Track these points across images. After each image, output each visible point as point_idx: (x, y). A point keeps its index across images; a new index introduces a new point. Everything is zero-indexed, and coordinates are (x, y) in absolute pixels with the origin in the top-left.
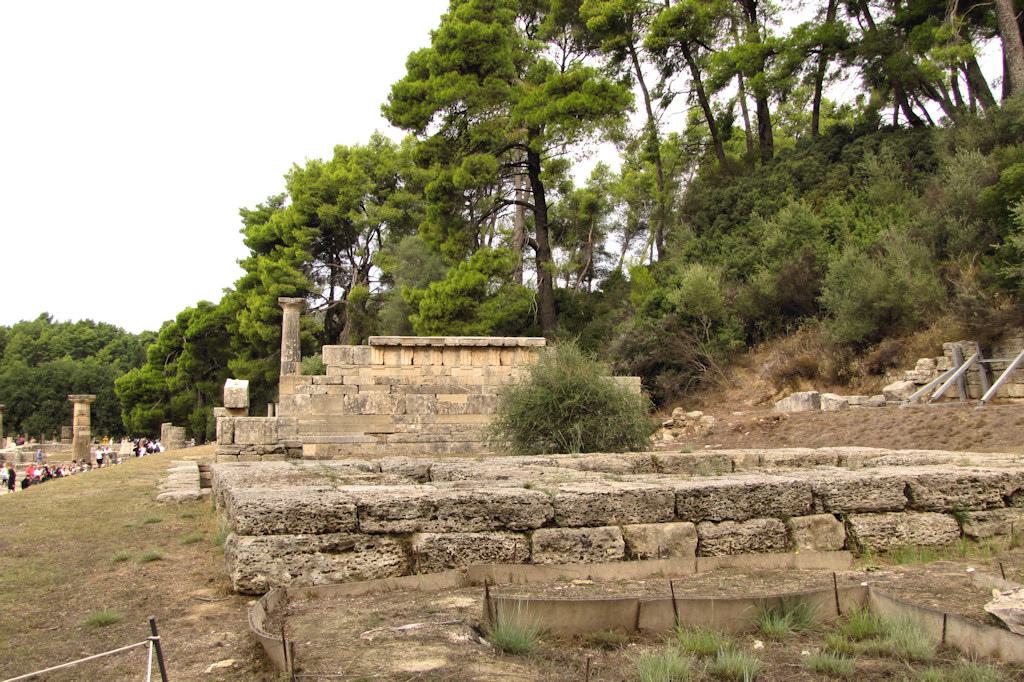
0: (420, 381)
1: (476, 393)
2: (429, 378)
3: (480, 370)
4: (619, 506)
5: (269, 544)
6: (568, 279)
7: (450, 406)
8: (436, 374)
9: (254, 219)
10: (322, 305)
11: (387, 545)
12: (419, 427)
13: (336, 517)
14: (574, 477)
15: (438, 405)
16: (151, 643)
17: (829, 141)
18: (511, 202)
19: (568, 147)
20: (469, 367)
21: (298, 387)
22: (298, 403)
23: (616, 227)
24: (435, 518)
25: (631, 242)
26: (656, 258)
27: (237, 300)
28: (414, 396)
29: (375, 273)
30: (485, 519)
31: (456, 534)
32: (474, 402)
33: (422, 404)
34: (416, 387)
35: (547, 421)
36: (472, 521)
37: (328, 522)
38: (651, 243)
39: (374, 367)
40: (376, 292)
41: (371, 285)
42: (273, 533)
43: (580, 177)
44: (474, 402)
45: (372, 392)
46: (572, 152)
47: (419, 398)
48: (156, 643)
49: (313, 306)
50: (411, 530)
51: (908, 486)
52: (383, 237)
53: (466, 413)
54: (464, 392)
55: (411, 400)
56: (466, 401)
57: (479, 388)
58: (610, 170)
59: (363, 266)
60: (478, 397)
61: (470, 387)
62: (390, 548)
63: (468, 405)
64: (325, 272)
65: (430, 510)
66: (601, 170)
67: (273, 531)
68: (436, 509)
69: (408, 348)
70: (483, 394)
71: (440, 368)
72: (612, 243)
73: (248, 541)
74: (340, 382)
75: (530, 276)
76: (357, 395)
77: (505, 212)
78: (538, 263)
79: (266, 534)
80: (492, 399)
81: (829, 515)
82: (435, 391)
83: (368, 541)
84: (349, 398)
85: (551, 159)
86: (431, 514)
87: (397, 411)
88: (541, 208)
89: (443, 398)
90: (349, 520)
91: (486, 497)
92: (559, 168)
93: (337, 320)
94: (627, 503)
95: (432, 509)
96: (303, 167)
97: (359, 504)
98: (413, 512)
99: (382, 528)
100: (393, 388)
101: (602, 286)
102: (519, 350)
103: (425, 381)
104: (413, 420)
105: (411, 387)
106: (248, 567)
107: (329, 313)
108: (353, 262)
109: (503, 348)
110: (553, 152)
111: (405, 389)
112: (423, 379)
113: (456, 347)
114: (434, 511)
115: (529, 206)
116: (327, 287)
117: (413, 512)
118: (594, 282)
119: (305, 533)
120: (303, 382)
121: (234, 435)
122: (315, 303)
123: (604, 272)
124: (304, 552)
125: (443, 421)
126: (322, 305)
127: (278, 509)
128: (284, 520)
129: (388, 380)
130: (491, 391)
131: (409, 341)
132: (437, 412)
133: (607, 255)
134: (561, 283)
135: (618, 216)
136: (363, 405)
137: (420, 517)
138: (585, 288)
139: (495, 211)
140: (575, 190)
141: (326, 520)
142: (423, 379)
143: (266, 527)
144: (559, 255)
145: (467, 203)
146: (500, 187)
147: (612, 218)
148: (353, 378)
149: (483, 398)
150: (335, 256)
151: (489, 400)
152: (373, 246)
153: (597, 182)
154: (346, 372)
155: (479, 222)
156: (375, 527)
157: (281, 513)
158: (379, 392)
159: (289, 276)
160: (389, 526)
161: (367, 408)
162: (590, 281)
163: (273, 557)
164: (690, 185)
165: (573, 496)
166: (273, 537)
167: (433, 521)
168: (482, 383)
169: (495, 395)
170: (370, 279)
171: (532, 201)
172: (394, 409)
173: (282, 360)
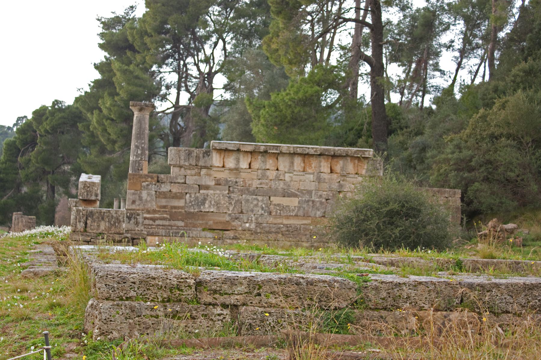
1: (307, 197)
2: (264, 181)
3: (312, 176)
4: (413, 295)
5: (123, 307)
6: (402, 94)
7: (283, 208)
8: (271, 178)
11: (219, 315)
12: (253, 226)
13: (179, 289)
15: (272, 206)
16: (45, 351)
21: (144, 184)
22: (144, 198)
23: (449, 47)
24: (259, 295)
28: (250, 198)
30: (300, 298)
31: (275, 309)
33: (257, 205)
34: (251, 189)
35: (389, 226)
36: (290, 298)
37: (171, 292)
38: (483, 60)
39: (215, 169)
41: (215, 91)
42: (127, 299)
44: (305, 206)
47: (254, 199)
48: (47, 350)
50: (239, 304)
52: (228, 47)
54: (295, 196)
55: (247, 201)
56: (297, 204)
57: (310, 192)
58: (393, 23)
60: (308, 201)
61: (301, 191)
62: (221, 318)
63: (299, 208)
64: (173, 78)
65: (255, 286)
67: (127, 298)
70: (313, 199)
71: (275, 173)
72: (447, 60)
74: (183, 181)
75: (364, 90)
76: (198, 194)
77: (344, 28)
78: (373, 78)
79: (122, 299)
80: (321, 203)
82: (269, 193)
83: (203, 310)
84: (190, 196)
86: (256, 292)
87: (233, 210)
89: (275, 200)
90: (189, 292)
91: (301, 280)
94: (419, 292)
95: (257, 287)
99: (215, 301)
100: (231, 189)
101: (436, 101)
102: (349, 159)
103: (261, 184)
104: (248, 220)
106: (106, 326)
107: (175, 116)
109: (334, 156)
111: (242, 191)
112: (258, 182)
114: (259, 289)
115: (367, 25)
116: (173, 91)
118: (428, 97)
119: (152, 301)
120: (149, 179)
121: (86, 224)
122: (161, 106)
123: (437, 88)
124: (152, 316)
125: (275, 222)
126: (168, 109)
127: (132, 280)
128: (136, 289)
129: (227, 181)
131: (249, 146)
132: (270, 213)
133: (443, 73)
134: (395, 98)
136: (203, 203)
137: (247, 293)
138: (417, 104)
140: (414, 8)
142: (258, 182)
144: (394, 71)
147: (444, 38)
149: (313, 201)
151: (318, 204)
154: (189, 172)
156: (209, 299)
157: (134, 283)
158: (218, 192)
160: (221, 299)
161: (207, 205)
162: (423, 97)
163: (126, 318)
165: (375, 283)
166: (127, 302)
167: (257, 297)
168: (313, 188)
169: (324, 200)
172: (231, 209)
173: (131, 158)
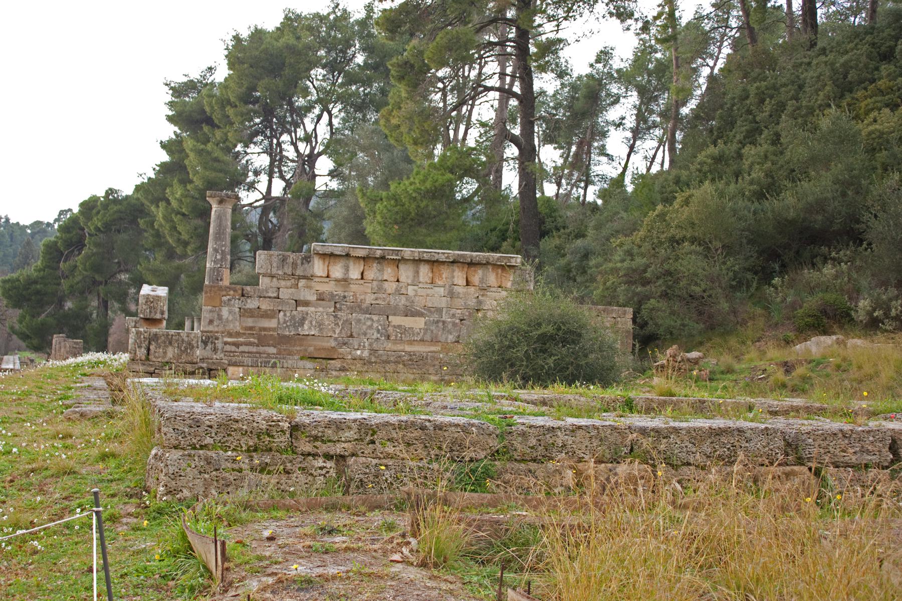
0: (369, 299)
1: (435, 317)
4: (570, 442)
5: (196, 458)
6: (559, 185)
7: (405, 330)
8: (389, 291)
9: (179, 91)
10: (257, 201)
11: (321, 468)
13: (269, 435)
14: (530, 408)
17: (883, 32)
18: (492, 89)
19: (565, 24)
20: (430, 286)
21: (224, 298)
22: (224, 317)
24: (373, 442)
25: (638, 143)
26: (666, 165)
27: (151, 190)
28: (362, 317)
29: (324, 165)
32: (433, 328)
33: (371, 327)
38: (661, 142)
39: (317, 279)
40: (324, 188)
42: (202, 447)
43: (579, 60)
45: (312, 309)
46: (569, 30)
49: (245, 201)
51: (894, 441)
52: (335, 122)
53: (422, 340)
54: (421, 315)
55: (359, 321)
56: (422, 326)
57: (439, 310)
59: (309, 156)
60: (438, 322)
61: (429, 309)
62: (324, 472)
65: (367, 431)
66: (604, 56)
68: (374, 433)
69: (427, 261)
70: (443, 319)
71: (395, 285)
72: (616, 142)
73: (176, 454)
74: (275, 295)
75: (511, 179)
78: (521, 164)
79: (195, 448)
80: (454, 324)
81: (802, 468)
82: (387, 312)
84: (285, 315)
85: (544, 38)
86: (368, 438)
87: (341, 332)
88: (528, 99)
89: (395, 320)
90: (282, 439)
91: (427, 424)
92: (551, 47)
93: (274, 220)
94: (578, 440)
95: (371, 432)
96: (245, 34)
97: (293, 424)
98: (350, 434)
101: (603, 194)
105: (359, 306)
106: (174, 483)
107: (265, 210)
108: (297, 150)
109: (472, 264)
110: (548, 31)
111: (352, 308)
112: (373, 296)
113: (414, 260)
114: (372, 435)
115: (515, 95)
116: (264, 178)
117: (350, 434)
119: (234, 450)
120: (232, 292)
121: (148, 350)
122: (247, 197)
123: (603, 178)
126: (257, 201)
127: (208, 423)
128: (213, 435)
129: (332, 295)
130: (454, 315)
131: (361, 251)
132: (388, 337)
134: (550, 189)
135: (625, 108)
136: (302, 324)
137: (357, 439)
138: (578, 198)
139: (473, 98)
141: (258, 437)
142: (373, 296)
143: (194, 441)
144: (550, 156)
145: (440, 85)
146: (481, 68)
147: (613, 114)
148: (290, 291)
149: (444, 322)
150: (275, 141)
151: (450, 326)
152: (323, 132)
153: (600, 66)
154: (283, 283)
155: (453, 110)
156: (308, 448)
157: (211, 427)
158: (321, 309)
159: (219, 161)
160: (324, 448)
161: (306, 327)
163: (200, 472)
164: (711, 78)
166: (201, 452)
168: (443, 305)
169: (458, 321)
170: (317, 172)
171: (517, 89)
172: (337, 331)
173: (208, 265)
